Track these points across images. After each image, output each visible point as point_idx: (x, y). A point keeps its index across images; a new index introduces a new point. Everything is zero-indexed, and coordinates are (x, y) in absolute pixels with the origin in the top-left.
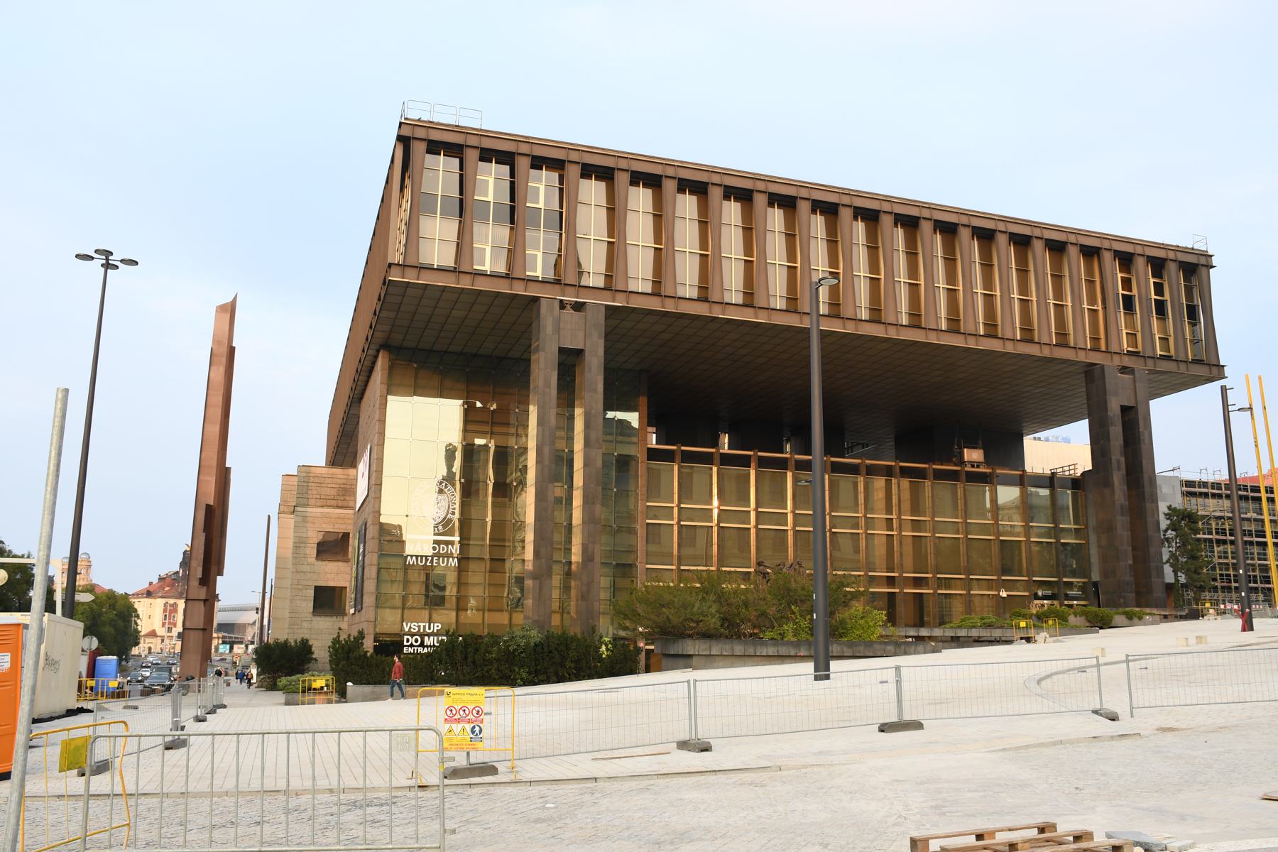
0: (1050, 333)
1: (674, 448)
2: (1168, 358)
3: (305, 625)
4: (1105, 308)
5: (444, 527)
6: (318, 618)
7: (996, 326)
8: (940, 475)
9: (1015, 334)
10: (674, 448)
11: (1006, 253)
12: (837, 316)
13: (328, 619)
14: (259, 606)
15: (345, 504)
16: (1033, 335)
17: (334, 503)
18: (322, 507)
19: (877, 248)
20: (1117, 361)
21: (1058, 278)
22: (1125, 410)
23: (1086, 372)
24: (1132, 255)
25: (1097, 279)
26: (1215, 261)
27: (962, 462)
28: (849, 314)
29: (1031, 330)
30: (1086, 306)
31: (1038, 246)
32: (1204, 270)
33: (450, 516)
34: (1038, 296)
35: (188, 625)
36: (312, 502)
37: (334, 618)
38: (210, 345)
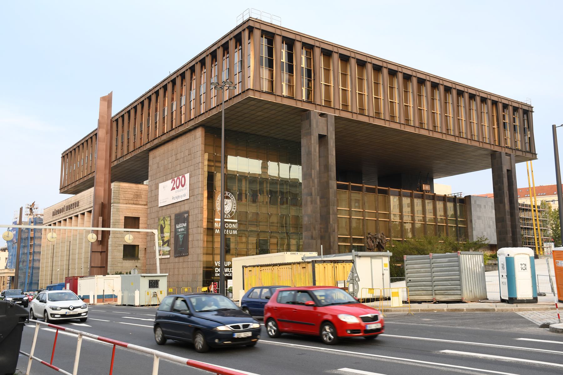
0: (321, 99)
1: (348, 183)
2: (507, 147)
3: (119, 265)
4: (498, 127)
5: (231, 215)
6: (125, 261)
7: (330, 102)
8: (354, 188)
9: (321, 102)
10: (348, 183)
11: (426, 90)
12: (292, 98)
13: (130, 261)
14: (369, 259)
15: (137, 202)
16: (330, 105)
17: (132, 202)
18: (126, 204)
19: (329, 70)
20: (319, 111)
21: (344, 75)
22: (508, 170)
23: (491, 155)
24: (475, 95)
25: (495, 114)
26: (534, 110)
27: (421, 190)
28: (279, 94)
29: (347, 106)
30: (341, 87)
31: (336, 56)
32: (530, 113)
33: (233, 210)
34: (334, 84)
35: (93, 265)
36: (121, 201)
37: (133, 261)
38: (97, 117)
